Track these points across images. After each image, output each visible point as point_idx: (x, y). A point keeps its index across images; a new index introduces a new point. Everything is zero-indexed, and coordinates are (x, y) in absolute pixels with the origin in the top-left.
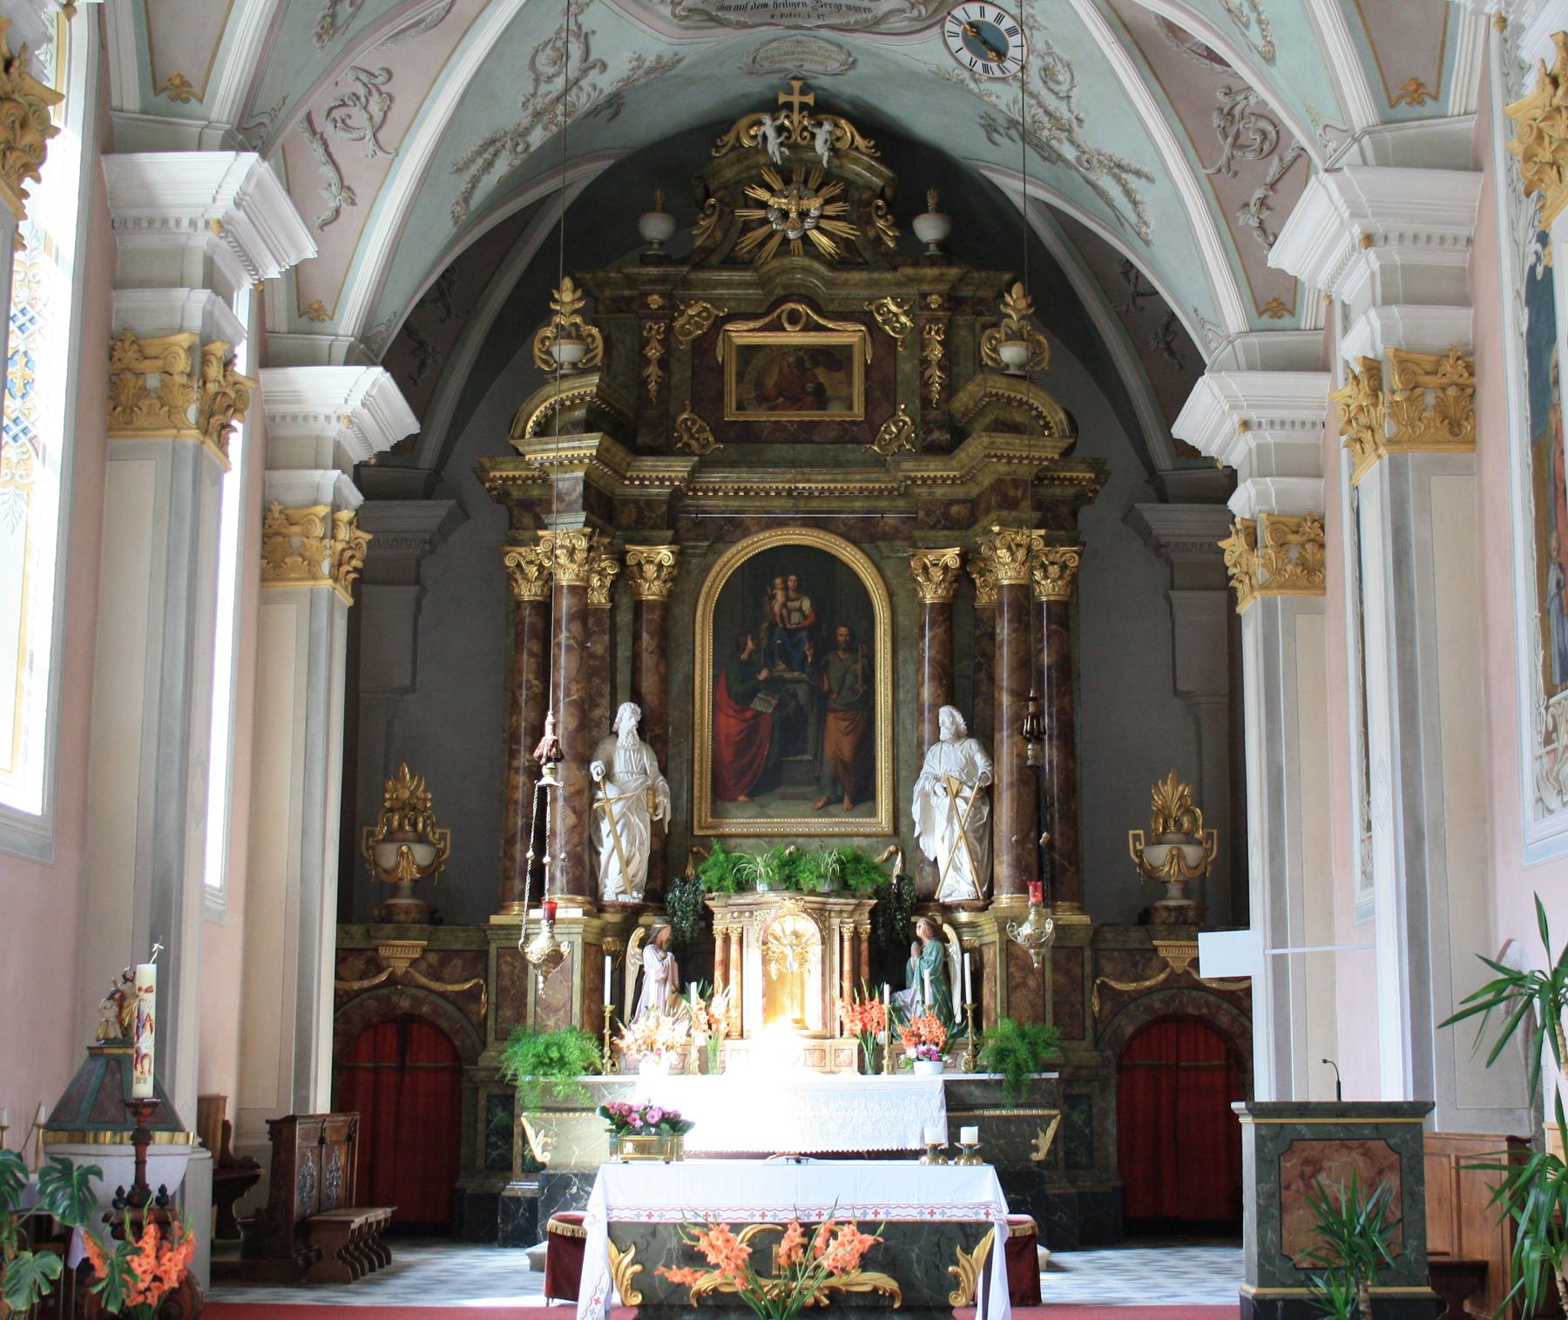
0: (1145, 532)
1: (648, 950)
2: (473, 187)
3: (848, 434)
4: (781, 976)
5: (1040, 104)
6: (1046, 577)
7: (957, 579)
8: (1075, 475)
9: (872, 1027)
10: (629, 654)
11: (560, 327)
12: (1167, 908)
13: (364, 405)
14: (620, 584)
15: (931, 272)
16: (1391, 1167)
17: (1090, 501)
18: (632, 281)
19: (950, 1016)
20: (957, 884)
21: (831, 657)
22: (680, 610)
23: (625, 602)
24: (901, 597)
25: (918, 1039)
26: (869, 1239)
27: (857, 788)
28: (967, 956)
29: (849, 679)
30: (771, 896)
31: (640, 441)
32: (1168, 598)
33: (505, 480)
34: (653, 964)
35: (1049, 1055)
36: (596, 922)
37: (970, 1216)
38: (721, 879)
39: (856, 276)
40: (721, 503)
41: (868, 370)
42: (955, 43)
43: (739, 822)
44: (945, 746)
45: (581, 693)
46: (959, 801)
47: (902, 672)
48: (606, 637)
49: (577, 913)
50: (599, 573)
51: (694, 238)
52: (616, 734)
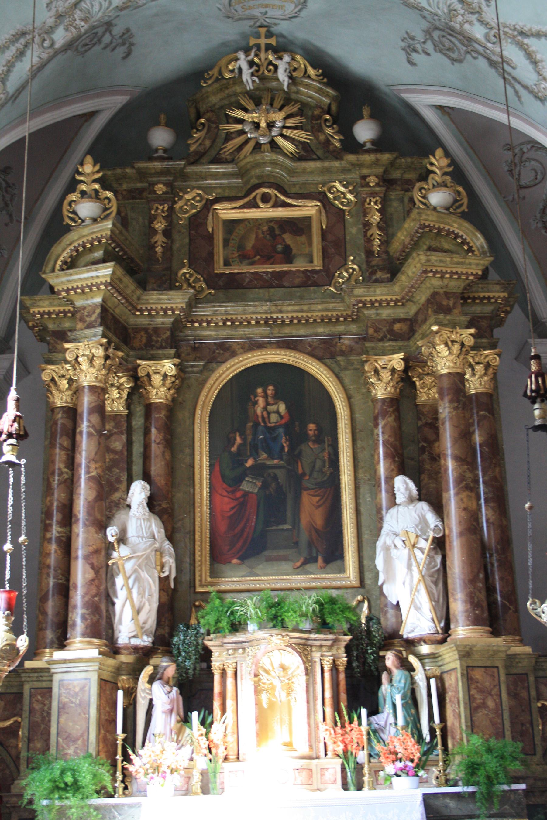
2: (9, 71)
3: (310, 281)
4: (272, 705)
6: (474, 375)
7: (402, 379)
8: (491, 295)
9: (352, 748)
10: (142, 450)
11: (83, 193)
14: (135, 397)
15: (368, 158)
18: (142, 175)
19: (420, 739)
20: (418, 621)
21: (303, 447)
22: (182, 415)
23: (139, 410)
24: (357, 399)
25: (395, 757)
27: (331, 552)
28: (433, 682)
29: (319, 464)
30: (262, 634)
33: (42, 314)
34: (159, 696)
35: (516, 767)
36: (111, 662)
38: (217, 621)
39: (311, 165)
40: (213, 333)
41: (324, 234)
43: (232, 580)
44: (401, 508)
45: (99, 471)
47: (360, 456)
48: (124, 437)
49: (94, 653)
50: (118, 388)
51: (189, 145)
52: (129, 506)
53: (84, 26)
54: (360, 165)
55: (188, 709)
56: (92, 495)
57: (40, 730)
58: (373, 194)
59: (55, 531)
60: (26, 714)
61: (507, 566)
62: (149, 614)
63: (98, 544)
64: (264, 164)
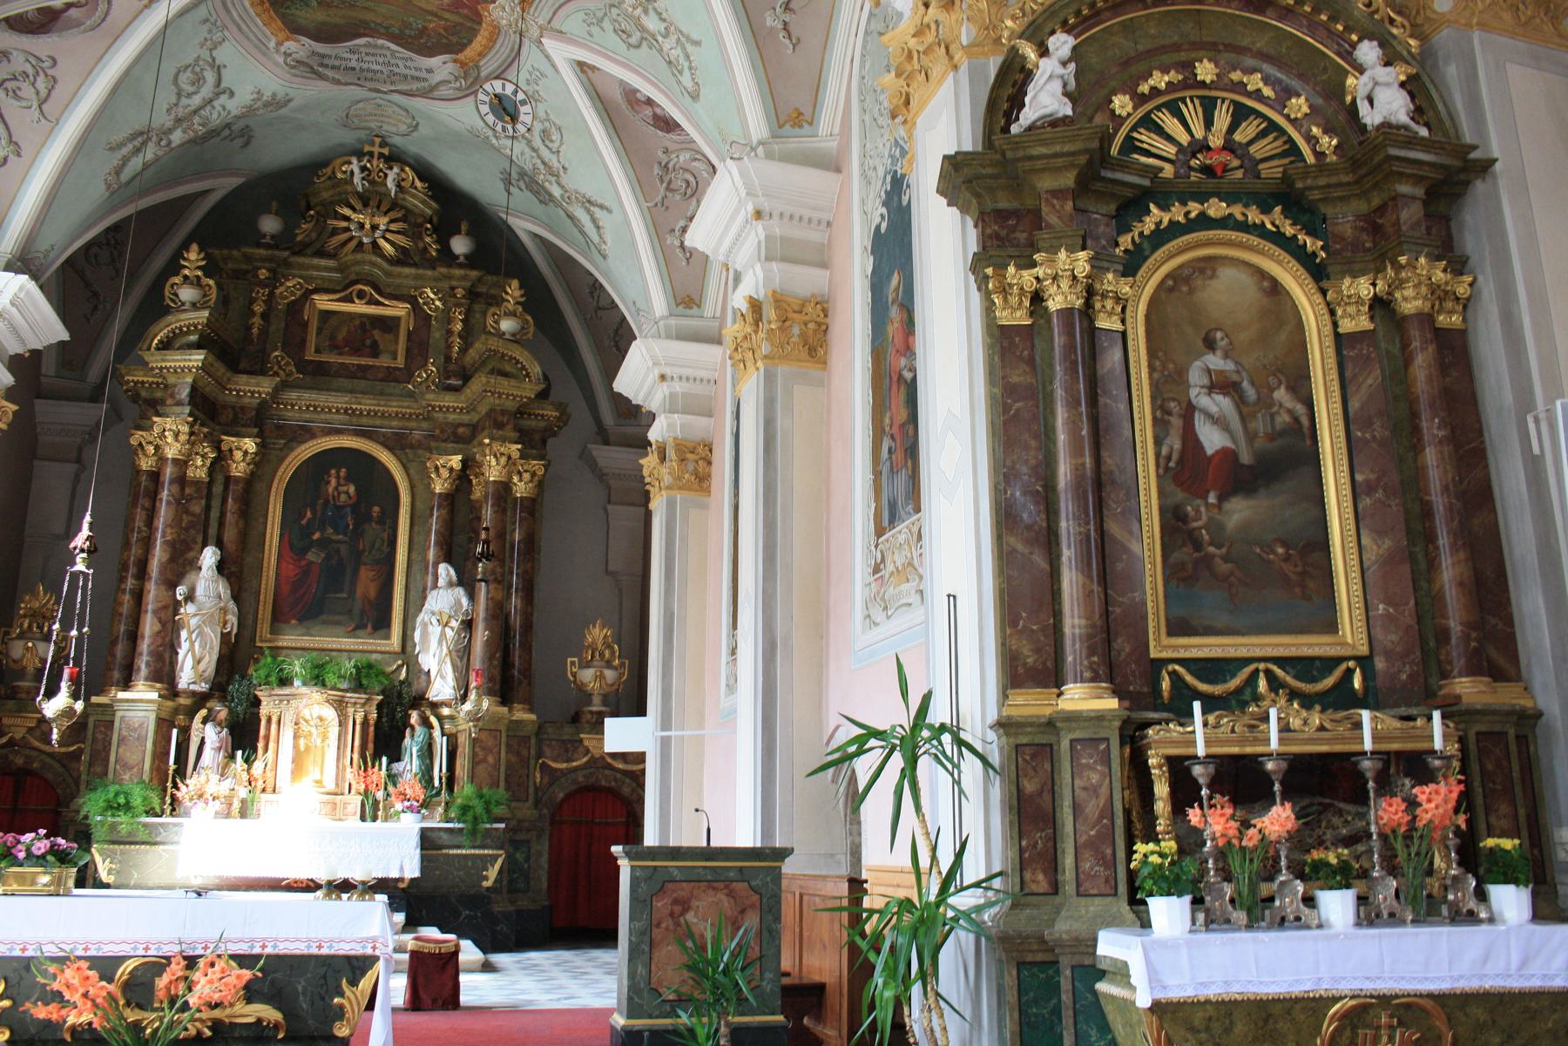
0: (593, 465)
1: (209, 727)
2: (124, 165)
3: (391, 376)
4: (308, 748)
5: (539, 157)
9: (372, 788)
11: (186, 277)
12: (591, 712)
13: (12, 304)
14: (218, 467)
15: (458, 272)
16: (752, 906)
17: (555, 434)
18: (248, 258)
20: (442, 688)
21: (367, 527)
23: (220, 478)
24: (420, 489)
25: (403, 796)
26: (247, 974)
30: (304, 690)
31: (242, 366)
32: (606, 510)
34: (210, 736)
35: (498, 811)
36: (170, 704)
37: (357, 950)
38: (268, 676)
39: (407, 270)
42: (485, 109)
43: (287, 640)
46: (448, 630)
47: (416, 539)
49: (154, 696)
53: (201, 130)
54: (450, 278)
55: (235, 748)
56: (166, 557)
57: (101, 756)
58: (458, 305)
59: (130, 583)
60: (89, 742)
61: (527, 647)
62: (209, 663)
63: (167, 601)
64: (364, 263)
